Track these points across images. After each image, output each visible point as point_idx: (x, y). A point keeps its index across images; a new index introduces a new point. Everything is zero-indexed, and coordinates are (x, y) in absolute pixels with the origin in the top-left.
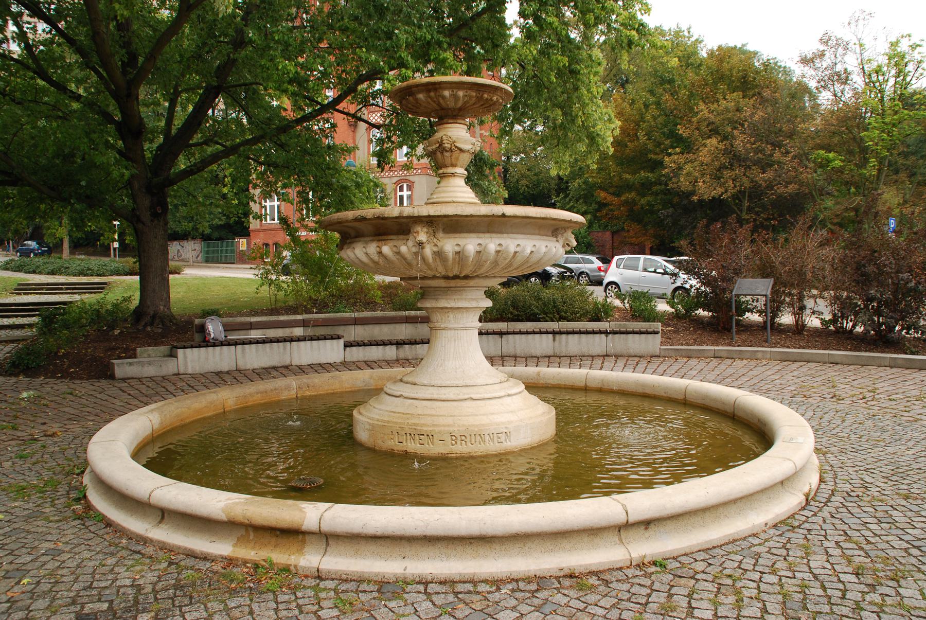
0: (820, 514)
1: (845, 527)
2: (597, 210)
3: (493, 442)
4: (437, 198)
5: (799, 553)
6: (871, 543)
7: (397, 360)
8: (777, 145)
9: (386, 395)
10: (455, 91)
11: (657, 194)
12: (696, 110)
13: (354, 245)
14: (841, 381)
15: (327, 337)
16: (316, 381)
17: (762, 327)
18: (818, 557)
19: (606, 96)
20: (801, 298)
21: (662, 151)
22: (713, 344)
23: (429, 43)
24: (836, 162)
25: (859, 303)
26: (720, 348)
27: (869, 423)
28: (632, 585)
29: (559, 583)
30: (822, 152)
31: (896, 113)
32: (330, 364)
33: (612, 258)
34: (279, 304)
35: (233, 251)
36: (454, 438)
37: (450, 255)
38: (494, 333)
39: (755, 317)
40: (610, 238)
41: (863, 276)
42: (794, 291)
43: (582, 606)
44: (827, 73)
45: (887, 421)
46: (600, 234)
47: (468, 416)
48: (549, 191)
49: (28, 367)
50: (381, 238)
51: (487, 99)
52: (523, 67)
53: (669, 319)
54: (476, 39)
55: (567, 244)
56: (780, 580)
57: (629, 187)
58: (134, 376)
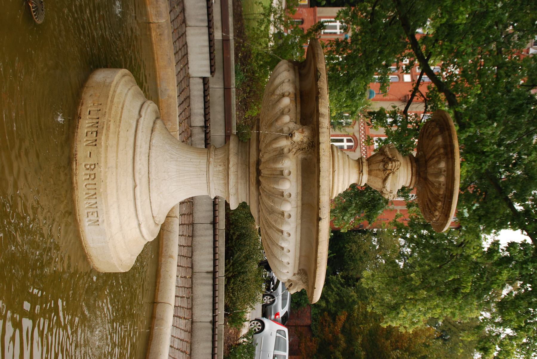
2: (329, 312)
3: (88, 208)
4: (338, 156)
7: (191, 126)
9: (142, 102)
10: (445, 173)
13: (292, 71)
15: (213, 62)
19: (433, 321)
32: (187, 63)
33: (286, 326)
34: (245, 22)
36: (93, 167)
37: (279, 166)
38: (215, 217)
40: (305, 324)
46: (309, 315)
47: (117, 182)
48: (347, 270)
50: (298, 96)
51: (436, 205)
52: (460, 245)
54: (486, 203)
55: (291, 284)
57: (350, 341)
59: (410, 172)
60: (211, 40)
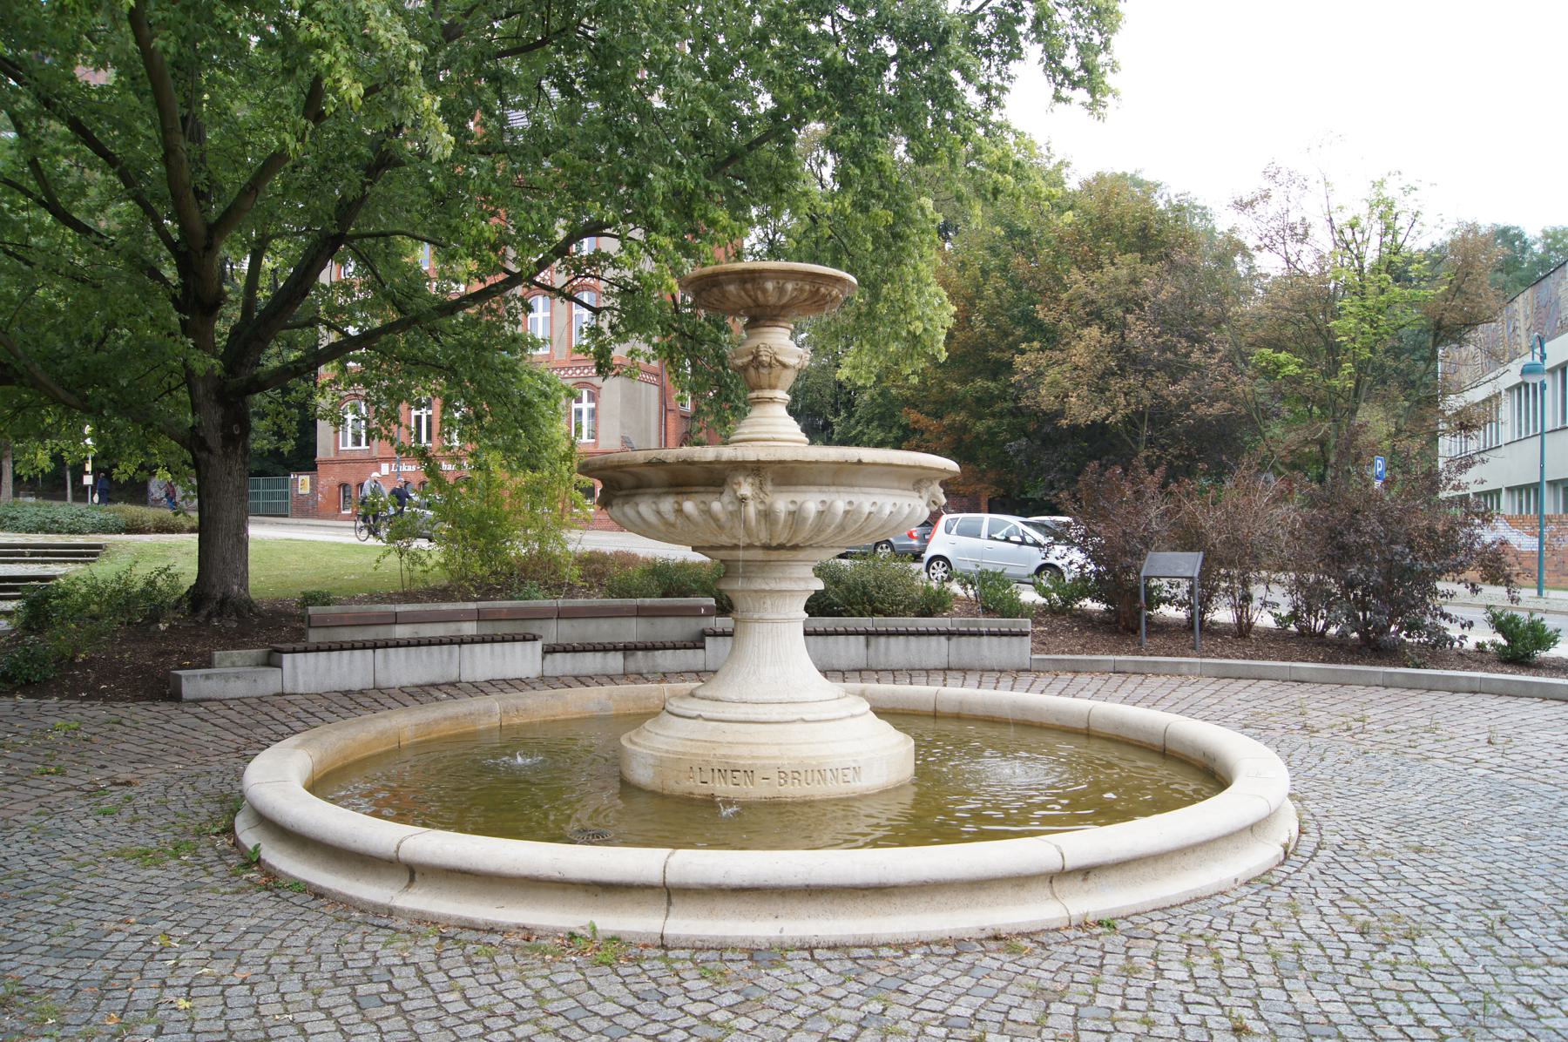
0: (1304, 870)
1: (1341, 885)
5: (1284, 913)
6: (1375, 901)
8: (1196, 339)
11: (1001, 415)
12: (1066, 281)
13: (637, 499)
14: (1313, 706)
15: (345, 646)
16: (529, 701)
17: (1188, 627)
18: (1310, 917)
20: (1245, 583)
21: (1010, 346)
22: (1111, 652)
23: (693, 194)
24: (1291, 367)
25: (1334, 591)
26: (1123, 658)
27: (1360, 762)
28: (1077, 947)
29: (982, 945)
30: (1267, 351)
31: (1383, 291)
32: (520, 679)
35: (286, 496)
39: (1168, 612)
41: (1339, 549)
42: (1235, 572)
43: (1021, 970)
44: (1273, 224)
45: (1385, 760)
49: (28, 682)
50: (680, 489)
53: (1038, 614)
56: (1266, 940)
57: (955, 403)
58: (212, 696)
59: (771, 329)
60: (483, 640)
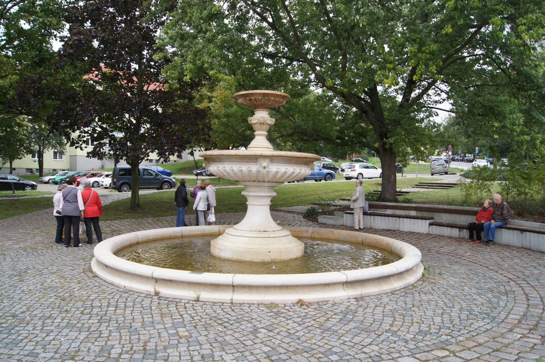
16: (322, 231)
